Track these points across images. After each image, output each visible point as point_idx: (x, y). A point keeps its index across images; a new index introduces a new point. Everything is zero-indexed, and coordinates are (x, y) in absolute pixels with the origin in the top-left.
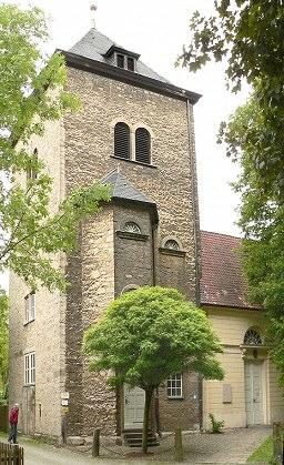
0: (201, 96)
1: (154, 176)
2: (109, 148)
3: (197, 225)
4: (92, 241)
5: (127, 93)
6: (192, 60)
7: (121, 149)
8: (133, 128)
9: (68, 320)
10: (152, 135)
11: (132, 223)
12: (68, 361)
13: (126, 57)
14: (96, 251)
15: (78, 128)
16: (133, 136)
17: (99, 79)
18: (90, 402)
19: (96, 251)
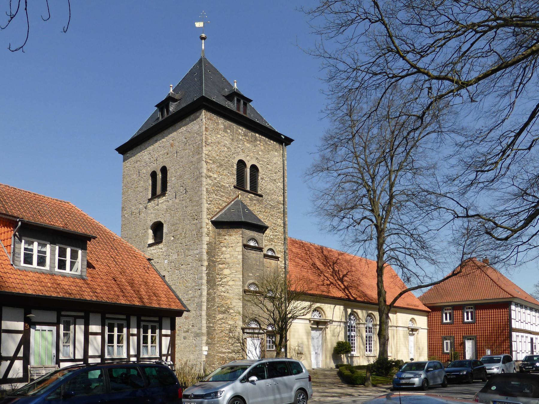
1: (260, 202)
2: (233, 180)
4: (224, 249)
6: (344, 243)
7: (240, 185)
8: (249, 166)
11: (253, 239)
13: (242, 101)
14: (228, 256)
16: (248, 171)
17: (228, 123)
19: (228, 256)
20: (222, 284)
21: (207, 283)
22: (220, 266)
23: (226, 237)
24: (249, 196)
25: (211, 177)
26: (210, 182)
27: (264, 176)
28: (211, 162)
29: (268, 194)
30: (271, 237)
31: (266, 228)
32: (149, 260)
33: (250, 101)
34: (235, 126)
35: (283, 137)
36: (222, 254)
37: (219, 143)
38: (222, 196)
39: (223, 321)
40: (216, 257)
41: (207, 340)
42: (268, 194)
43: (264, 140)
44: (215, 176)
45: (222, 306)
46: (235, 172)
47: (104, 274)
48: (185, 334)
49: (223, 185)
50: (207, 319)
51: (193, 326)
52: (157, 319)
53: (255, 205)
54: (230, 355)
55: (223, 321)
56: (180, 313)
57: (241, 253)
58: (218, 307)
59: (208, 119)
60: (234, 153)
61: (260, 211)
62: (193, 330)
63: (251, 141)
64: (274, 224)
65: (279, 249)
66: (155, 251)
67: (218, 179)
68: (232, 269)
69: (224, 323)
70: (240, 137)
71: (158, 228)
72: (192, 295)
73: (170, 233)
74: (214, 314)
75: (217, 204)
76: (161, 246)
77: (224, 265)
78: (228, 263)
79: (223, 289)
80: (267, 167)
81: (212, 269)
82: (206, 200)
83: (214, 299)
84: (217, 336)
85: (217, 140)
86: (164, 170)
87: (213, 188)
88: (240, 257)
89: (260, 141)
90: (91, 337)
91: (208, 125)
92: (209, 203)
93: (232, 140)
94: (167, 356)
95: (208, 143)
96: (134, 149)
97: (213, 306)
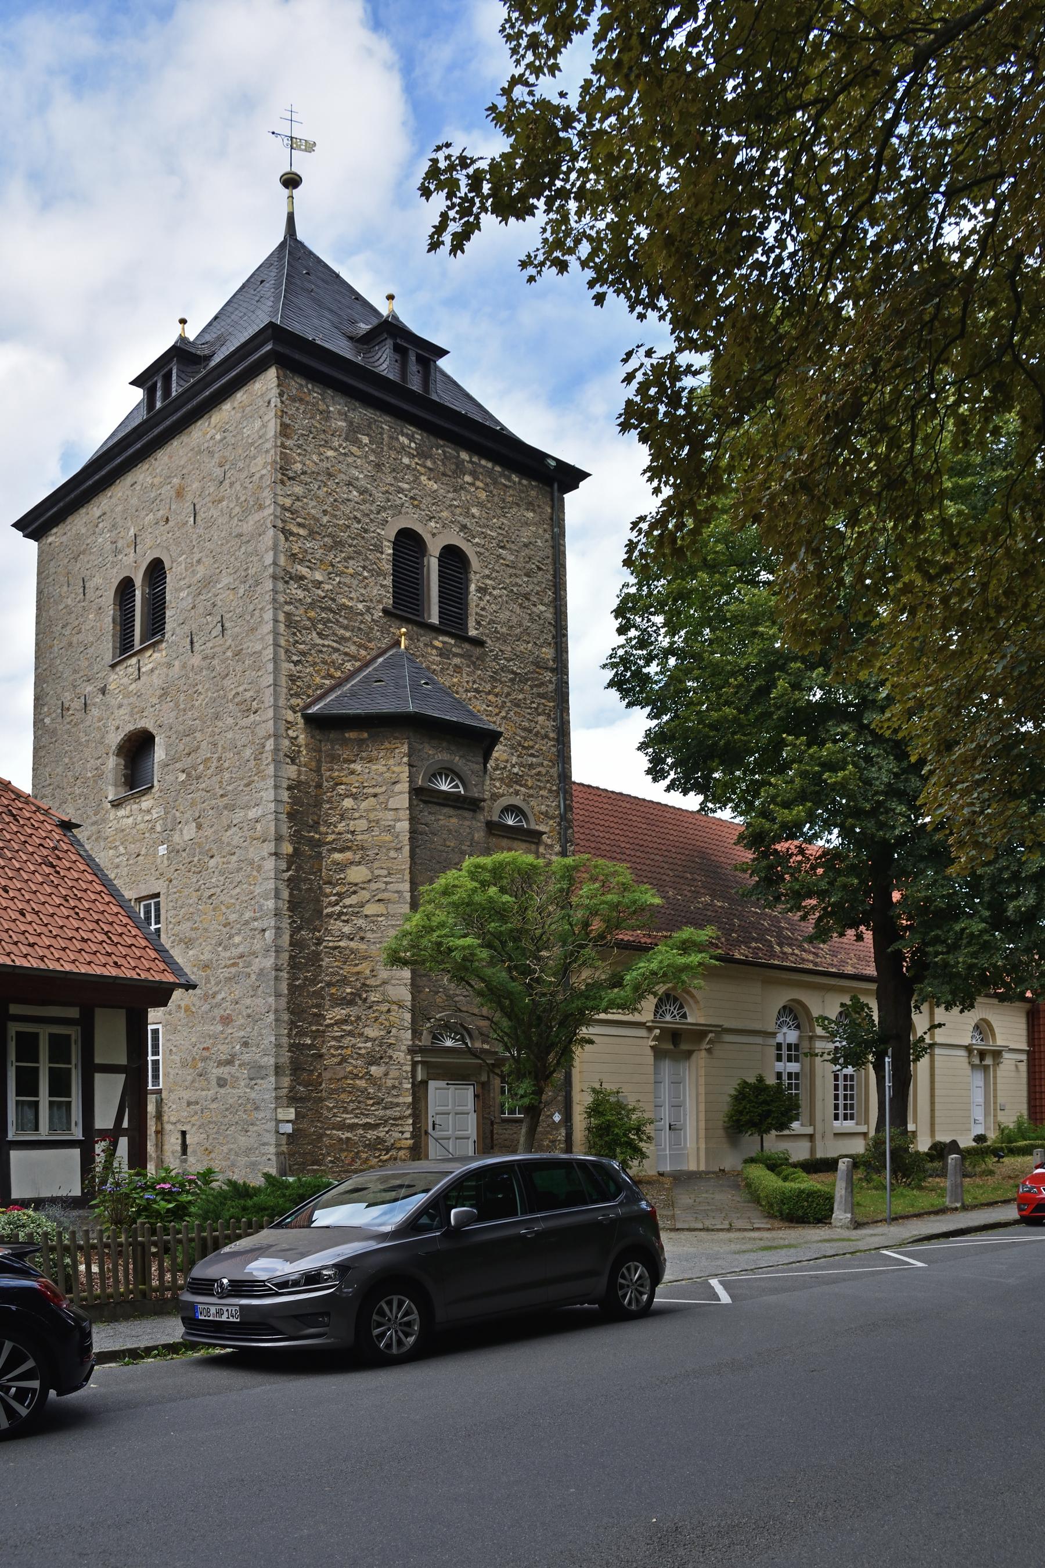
0: (585, 475)
1: (476, 663)
2: (381, 591)
3: (565, 774)
4: (348, 803)
5: (422, 454)
7: (406, 603)
8: (434, 548)
9: (294, 964)
10: (475, 563)
11: (449, 772)
12: (292, 1048)
14: (362, 824)
15: (312, 533)
16: (434, 563)
17: (361, 414)
18: (342, 1126)
19: (362, 824)
20: (341, 913)
21: (289, 909)
22: (337, 856)
23: (357, 767)
24: (436, 643)
25: (302, 578)
26: (301, 594)
27: (488, 582)
28: (302, 532)
29: (503, 639)
30: (515, 770)
31: (494, 737)
32: (67, 826)
33: (442, 353)
34: (385, 424)
35: (553, 463)
36: (342, 818)
37: (330, 475)
38: (343, 639)
39: (349, 1028)
40: (323, 829)
41: (292, 1089)
42: (503, 639)
43: (490, 473)
44: (318, 576)
45: (344, 981)
46: (388, 567)
47: (91, 925)
48: (221, 1070)
49: (344, 606)
50: (292, 1024)
51: (246, 1044)
52: (73, 1013)
53: (458, 669)
54: (371, 1135)
55: (349, 1028)
56: (160, 994)
57: (405, 814)
58: (329, 984)
59: (293, 399)
60: (385, 509)
61: (477, 691)
62: (246, 1057)
63: (444, 474)
64: (525, 729)
65: (543, 808)
66: (130, 820)
67: (327, 587)
68: (376, 864)
69: (350, 1033)
70: (406, 460)
71: (137, 748)
72: (241, 949)
73: (175, 760)
74: (317, 1006)
75: (324, 662)
76: (146, 803)
77: (349, 855)
78: (363, 848)
79: (347, 929)
80: (499, 556)
81: (307, 867)
82: (287, 651)
83: (316, 957)
84: (327, 1075)
85: (325, 464)
86: (156, 570)
87: (312, 614)
88: (404, 826)
89: (474, 474)
90: (98, 1077)
91: (292, 417)
92: (295, 658)
93: (378, 466)
94: (112, 1136)
95: (291, 474)
96: (70, 519)
97: (314, 981)
